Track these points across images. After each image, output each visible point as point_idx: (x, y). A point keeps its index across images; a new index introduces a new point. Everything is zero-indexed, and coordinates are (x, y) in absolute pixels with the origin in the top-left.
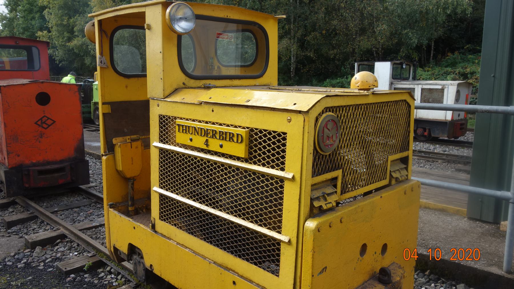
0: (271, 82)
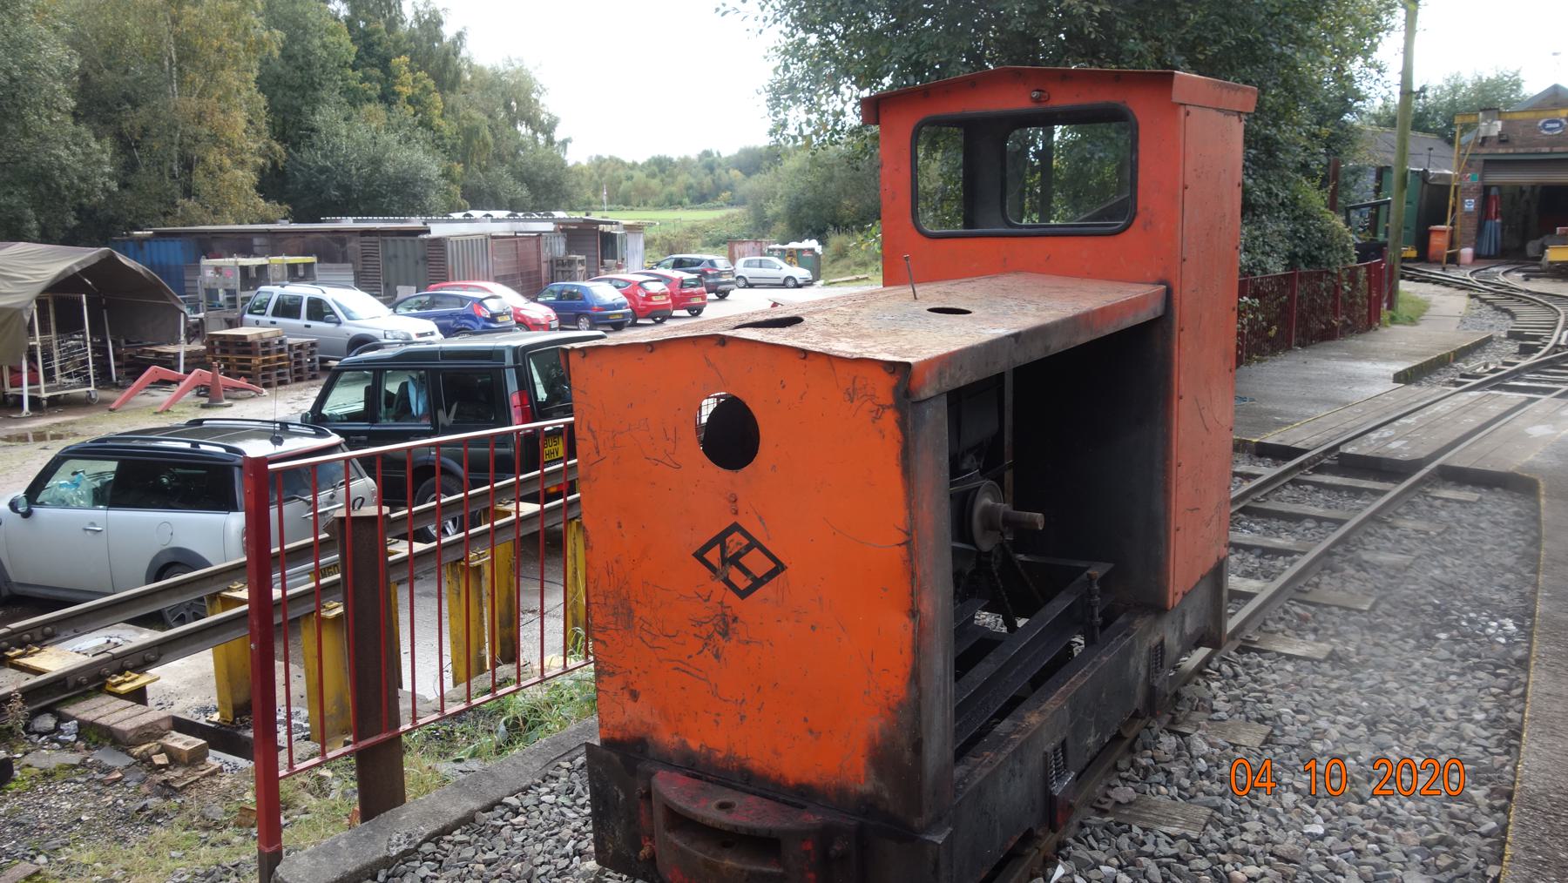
0: (1459, 73)
